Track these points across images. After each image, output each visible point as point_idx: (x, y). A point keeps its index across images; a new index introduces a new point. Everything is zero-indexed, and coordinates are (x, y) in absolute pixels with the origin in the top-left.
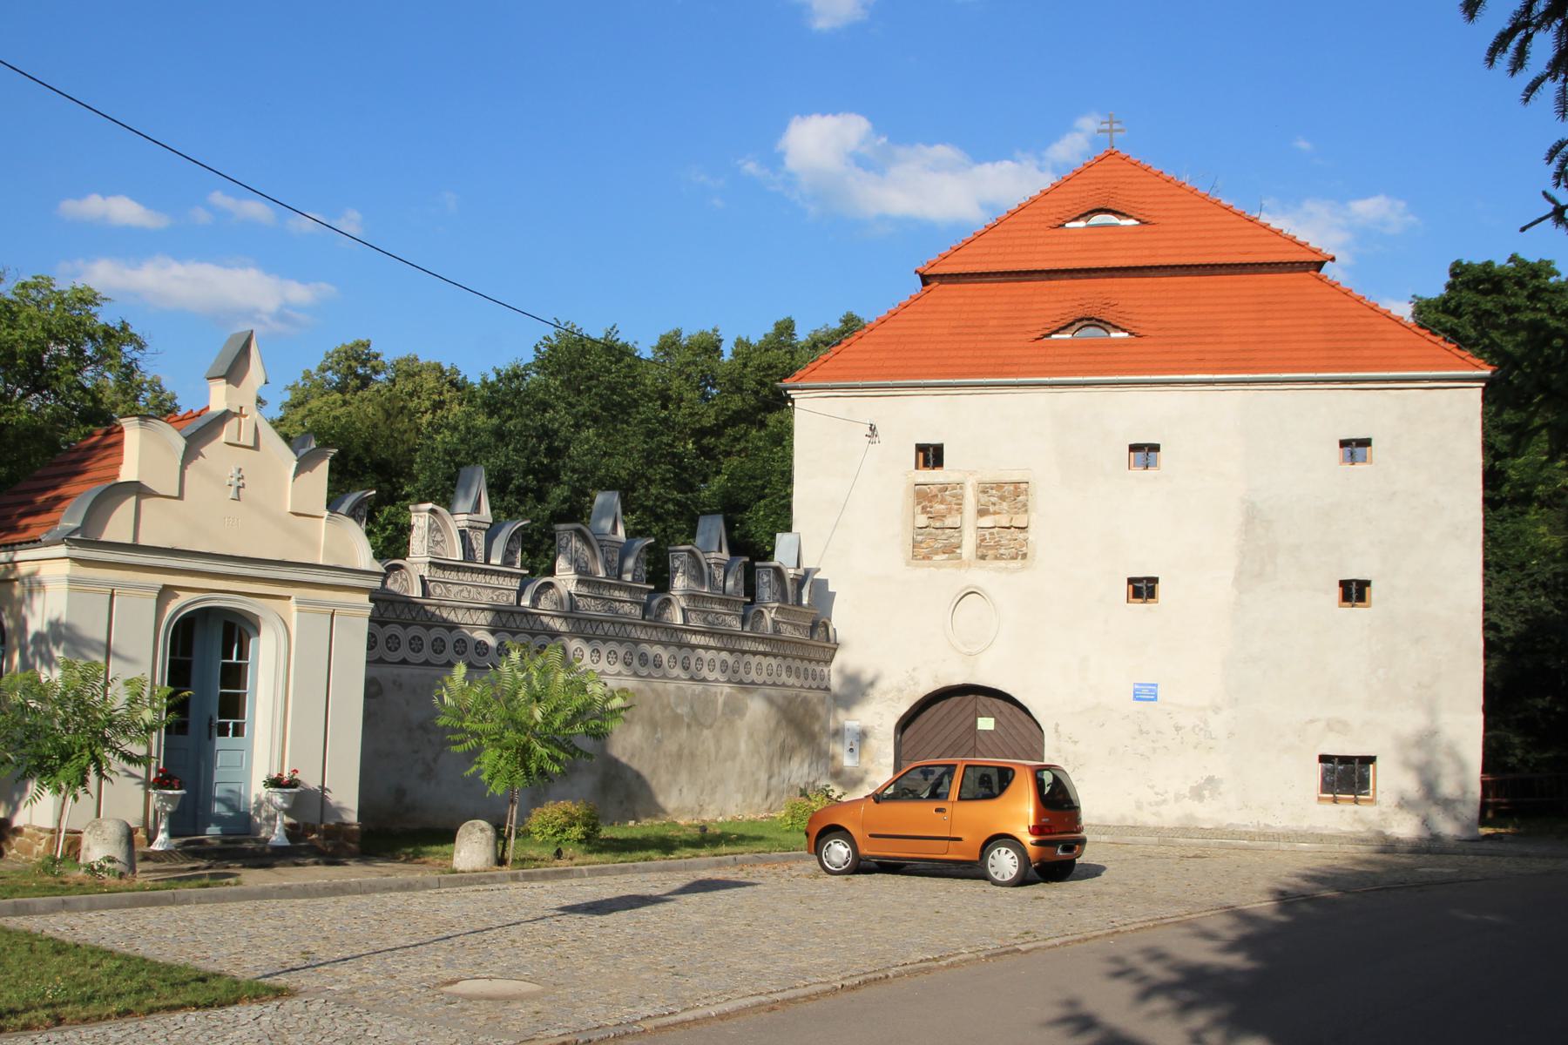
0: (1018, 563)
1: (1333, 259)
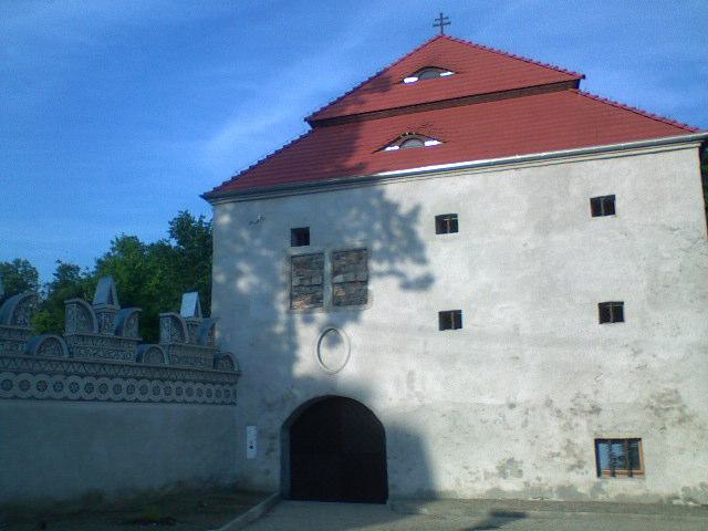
1: (584, 77)
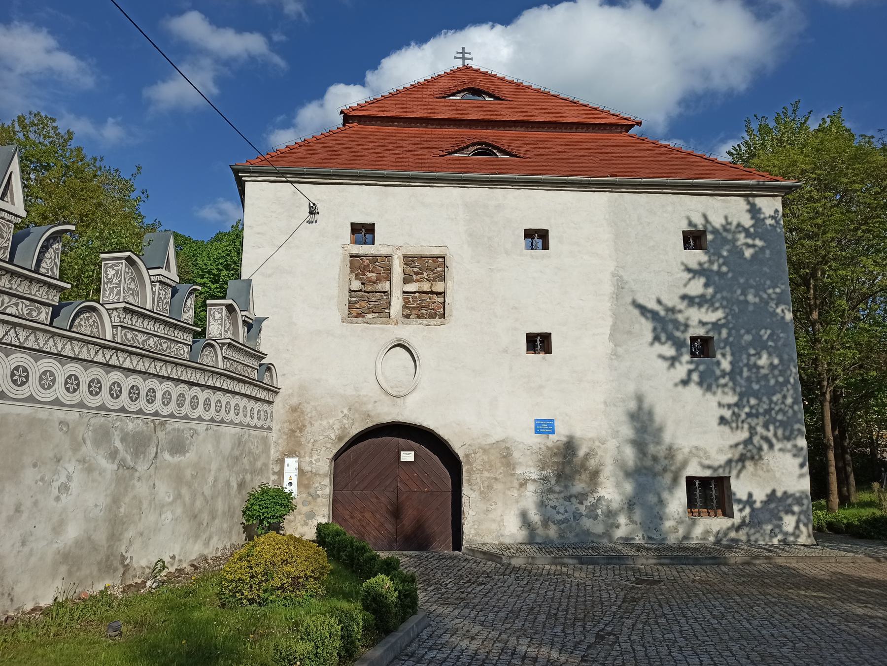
0: (438, 321)
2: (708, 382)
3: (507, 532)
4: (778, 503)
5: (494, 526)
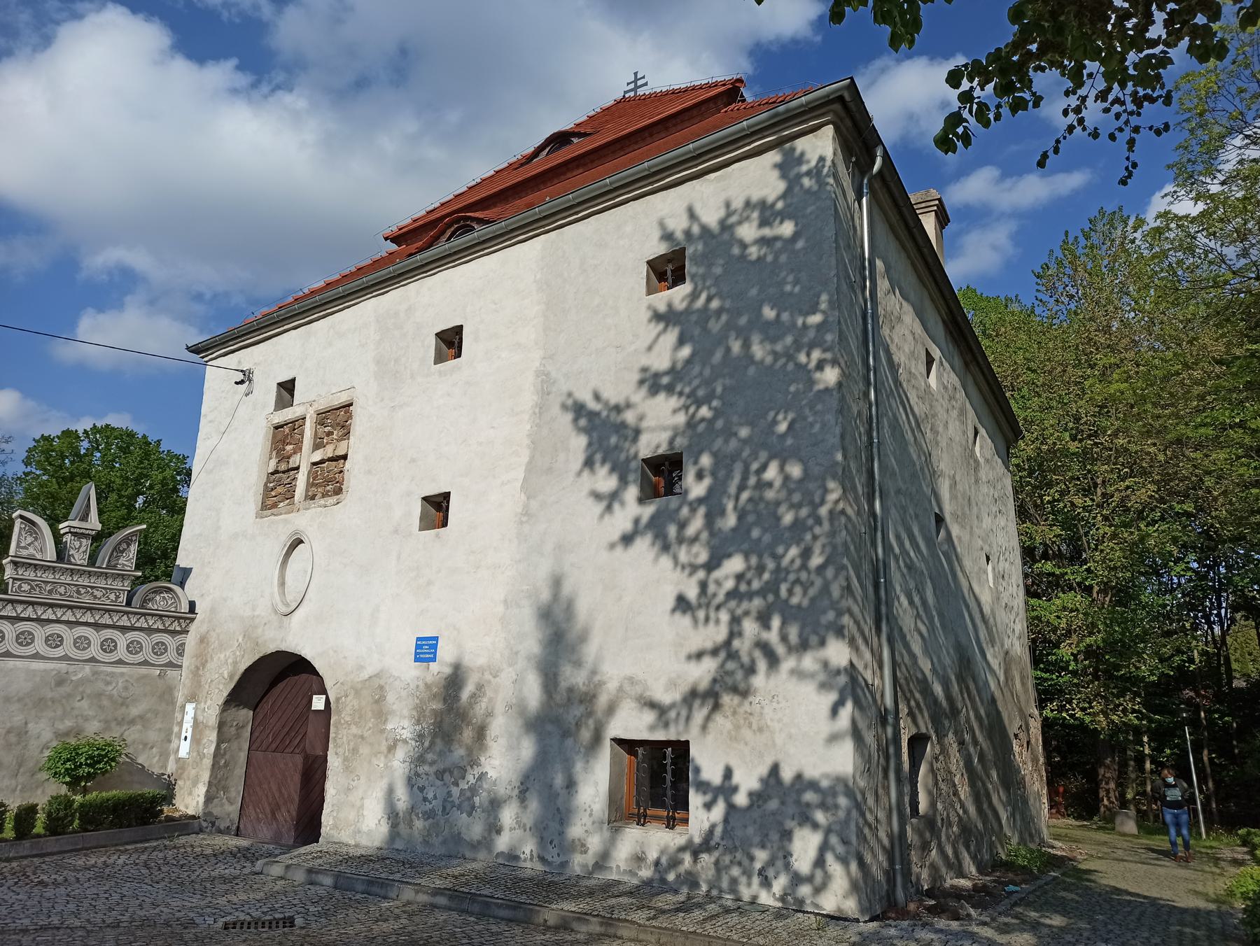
2: (660, 532)
3: (364, 828)
4: (784, 800)
5: (352, 816)
